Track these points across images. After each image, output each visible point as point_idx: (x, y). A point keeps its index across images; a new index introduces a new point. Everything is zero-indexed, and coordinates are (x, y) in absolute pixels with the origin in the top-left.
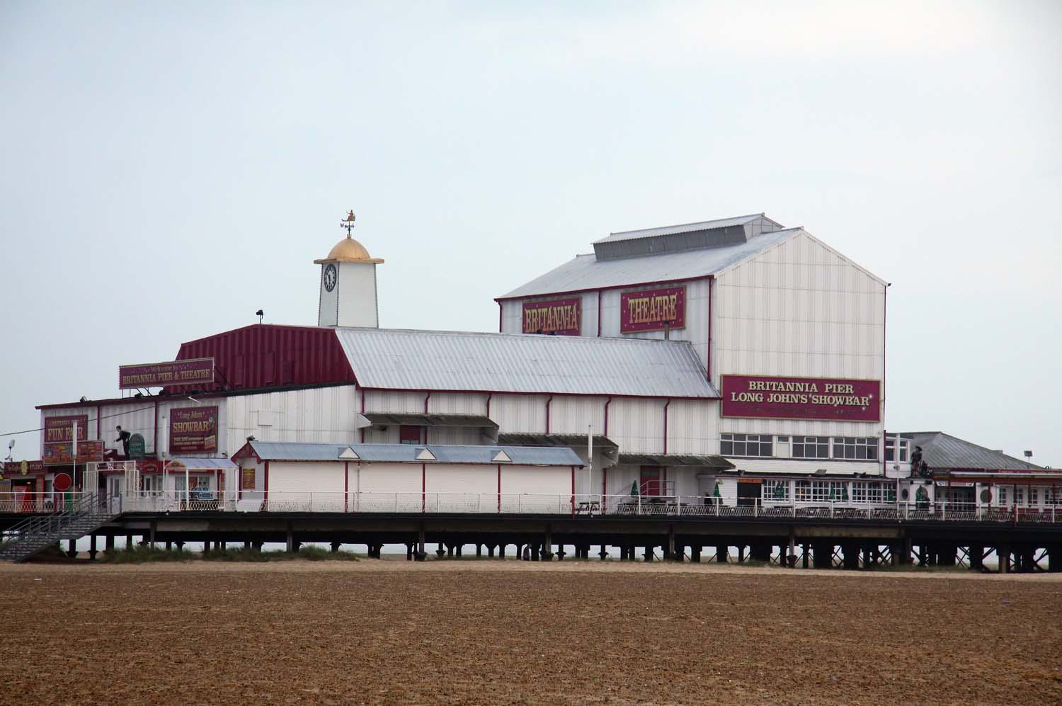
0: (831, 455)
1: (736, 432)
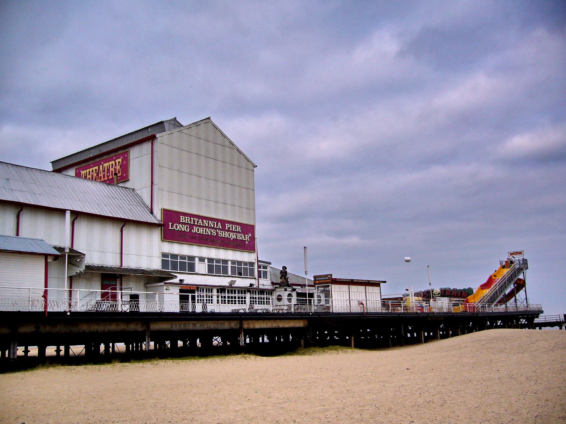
0: (230, 273)
1: (172, 253)
